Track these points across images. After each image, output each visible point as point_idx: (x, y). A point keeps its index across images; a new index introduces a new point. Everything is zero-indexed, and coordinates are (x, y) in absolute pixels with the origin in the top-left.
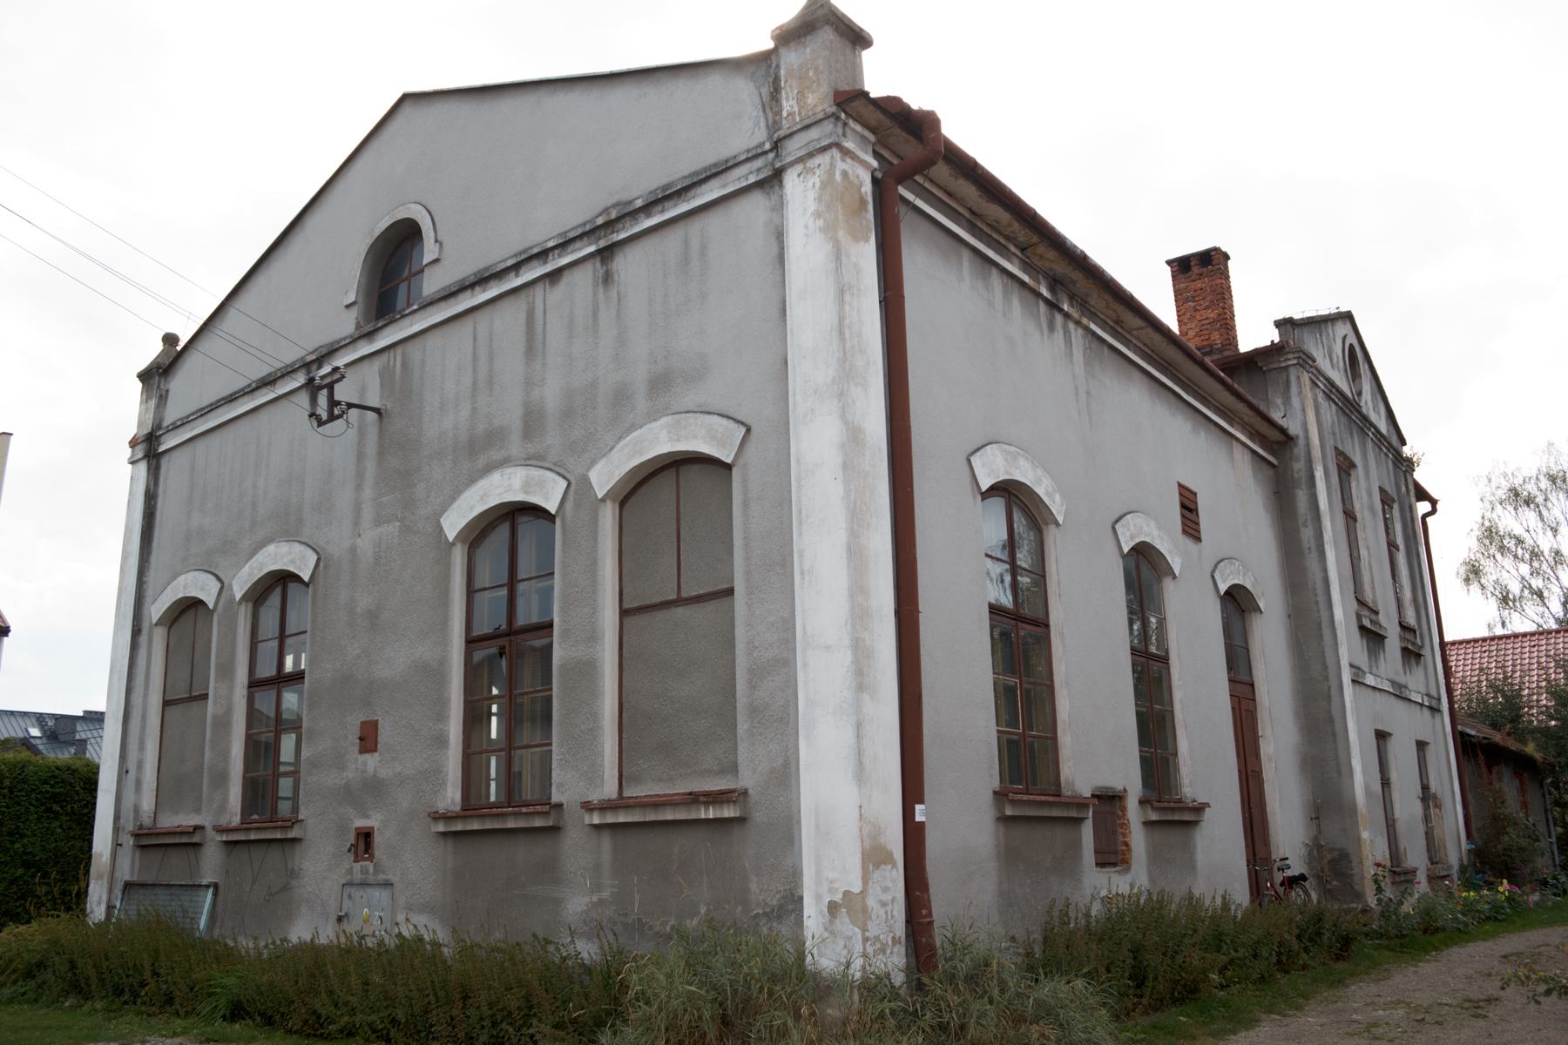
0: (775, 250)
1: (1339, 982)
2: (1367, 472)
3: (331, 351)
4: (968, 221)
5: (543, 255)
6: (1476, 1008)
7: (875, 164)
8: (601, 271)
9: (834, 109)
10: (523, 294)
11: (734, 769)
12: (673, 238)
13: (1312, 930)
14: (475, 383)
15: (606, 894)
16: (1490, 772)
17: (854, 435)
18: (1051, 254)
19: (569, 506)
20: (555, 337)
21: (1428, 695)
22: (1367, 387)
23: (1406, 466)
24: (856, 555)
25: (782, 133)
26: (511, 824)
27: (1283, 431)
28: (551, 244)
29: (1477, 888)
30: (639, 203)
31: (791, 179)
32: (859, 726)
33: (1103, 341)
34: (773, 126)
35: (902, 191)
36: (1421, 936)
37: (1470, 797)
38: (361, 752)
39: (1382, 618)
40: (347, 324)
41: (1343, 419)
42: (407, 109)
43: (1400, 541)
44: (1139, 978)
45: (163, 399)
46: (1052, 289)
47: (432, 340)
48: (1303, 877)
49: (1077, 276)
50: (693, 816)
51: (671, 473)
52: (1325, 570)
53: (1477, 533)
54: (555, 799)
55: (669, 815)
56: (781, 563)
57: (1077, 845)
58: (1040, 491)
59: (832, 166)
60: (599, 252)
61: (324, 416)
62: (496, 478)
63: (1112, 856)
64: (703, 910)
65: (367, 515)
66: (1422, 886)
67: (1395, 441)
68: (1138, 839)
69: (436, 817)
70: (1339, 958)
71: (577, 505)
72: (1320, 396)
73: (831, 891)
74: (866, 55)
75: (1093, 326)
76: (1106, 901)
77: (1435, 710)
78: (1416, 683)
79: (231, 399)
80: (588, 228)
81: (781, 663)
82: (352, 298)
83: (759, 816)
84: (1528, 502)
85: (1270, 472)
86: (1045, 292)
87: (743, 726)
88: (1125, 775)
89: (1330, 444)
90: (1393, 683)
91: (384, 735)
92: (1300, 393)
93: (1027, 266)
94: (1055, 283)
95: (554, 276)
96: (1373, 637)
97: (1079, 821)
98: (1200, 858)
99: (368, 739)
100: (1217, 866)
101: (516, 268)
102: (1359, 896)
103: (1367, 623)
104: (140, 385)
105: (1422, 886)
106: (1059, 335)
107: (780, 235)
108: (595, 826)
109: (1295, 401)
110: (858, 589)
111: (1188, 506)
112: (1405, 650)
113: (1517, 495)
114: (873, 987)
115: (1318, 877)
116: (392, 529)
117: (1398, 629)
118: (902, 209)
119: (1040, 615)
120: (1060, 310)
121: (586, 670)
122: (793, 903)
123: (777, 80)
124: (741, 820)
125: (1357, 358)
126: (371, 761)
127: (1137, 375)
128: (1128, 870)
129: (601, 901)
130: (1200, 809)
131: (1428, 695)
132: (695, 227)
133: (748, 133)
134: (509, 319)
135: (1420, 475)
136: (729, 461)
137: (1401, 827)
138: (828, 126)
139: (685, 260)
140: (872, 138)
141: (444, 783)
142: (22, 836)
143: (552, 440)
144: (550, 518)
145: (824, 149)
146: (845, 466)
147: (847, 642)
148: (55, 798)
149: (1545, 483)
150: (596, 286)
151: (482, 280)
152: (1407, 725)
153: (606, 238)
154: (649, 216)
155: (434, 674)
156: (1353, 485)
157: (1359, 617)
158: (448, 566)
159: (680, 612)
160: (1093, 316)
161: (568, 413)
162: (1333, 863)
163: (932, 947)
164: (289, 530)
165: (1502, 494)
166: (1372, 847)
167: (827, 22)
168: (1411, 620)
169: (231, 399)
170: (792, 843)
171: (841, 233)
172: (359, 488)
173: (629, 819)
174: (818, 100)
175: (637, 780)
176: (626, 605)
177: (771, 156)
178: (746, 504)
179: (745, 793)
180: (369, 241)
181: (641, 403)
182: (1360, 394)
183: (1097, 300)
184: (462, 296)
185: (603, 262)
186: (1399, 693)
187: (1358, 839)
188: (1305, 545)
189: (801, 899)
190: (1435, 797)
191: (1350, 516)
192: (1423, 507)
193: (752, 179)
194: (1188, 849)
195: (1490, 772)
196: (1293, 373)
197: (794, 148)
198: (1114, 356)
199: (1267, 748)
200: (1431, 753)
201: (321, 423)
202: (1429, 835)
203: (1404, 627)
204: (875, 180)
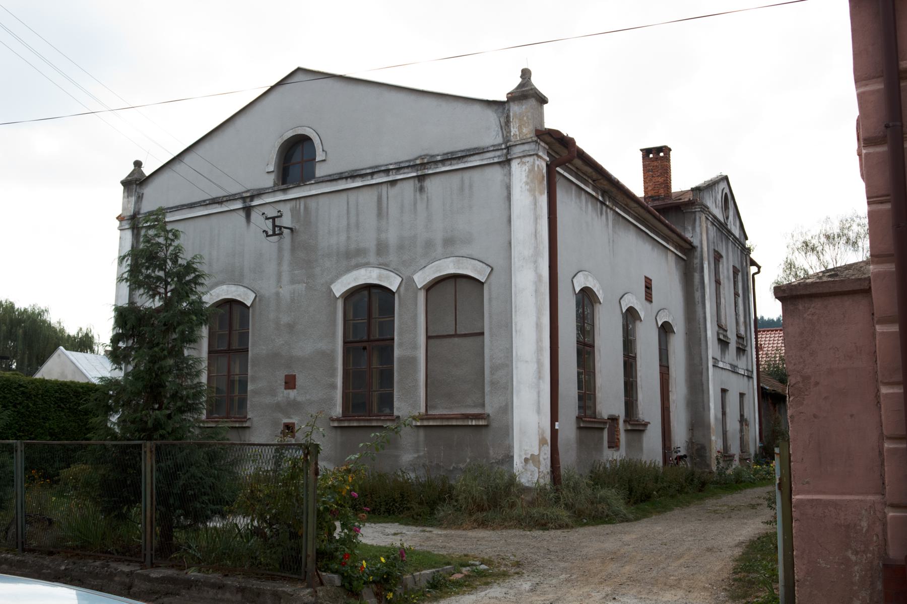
0: (505, 194)
1: (701, 499)
2: (728, 259)
3: (259, 193)
4: (576, 173)
5: (387, 171)
6: (753, 507)
7: (548, 159)
8: (418, 185)
9: (535, 139)
10: (375, 188)
11: (483, 405)
12: (455, 179)
13: (690, 478)
14: (348, 225)
15: (421, 454)
16: (775, 407)
17: (539, 277)
18: (605, 183)
19: (402, 289)
20: (393, 210)
21: (747, 370)
22: (731, 213)
23: (746, 251)
24: (538, 326)
25: (511, 143)
26: (374, 424)
27: (690, 243)
28: (391, 167)
29: (761, 465)
30: (439, 158)
31: (515, 164)
32: (539, 393)
33: (620, 215)
34: (506, 140)
35: (558, 169)
36: (737, 483)
37: (763, 419)
38: (286, 388)
39: (729, 334)
40: (269, 181)
41: (719, 234)
42: (300, 77)
43: (740, 292)
44: (631, 490)
45: (140, 198)
46: (603, 196)
47: (322, 200)
48: (685, 456)
49: (614, 190)
50: (466, 423)
51: (452, 282)
52: (705, 313)
53: (783, 266)
54: (396, 413)
55: (454, 423)
56: (507, 326)
57: (602, 438)
58: (595, 290)
59: (534, 163)
60: (418, 176)
61: (270, 233)
62: (362, 271)
63: (614, 444)
64: (468, 460)
65: (286, 278)
66: (736, 463)
67: (742, 240)
68: (622, 437)
69: (333, 420)
70: (700, 491)
71: (406, 289)
72: (709, 223)
73: (525, 454)
74: (545, 106)
75: (617, 210)
76: (611, 462)
77: (750, 377)
78: (742, 364)
79: (191, 206)
80: (412, 164)
81: (507, 364)
82: (272, 169)
83: (494, 425)
84: (813, 249)
85: (683, 263)
86: (600, 198)
87: (487, 389)
88: (619, 410)
89: (712, 248)
90: (731, 365)
91: (299, 381)
92: (700, 225)
93: (595, 188)
94: (604, 193)
95: (393, 183)
96: (723, 343)
97: (602, 429)
98: (645, 445)
99: (290, 382)
100: (651, 448)
101: (372, 174)
102: (709, 466)
103: (721, 337)
104: (122, 187)
105: (736, 463)
106: (604, 217)
107: (508, 188)
108: (417, 426)
109: (698, 229)
110: (539, 340)
111: (648, 287)
112: (738, 349)
113: (807, 245)
114: (542, 490)
115: (691, 457)
116: (301, 287)
117: (735, 337)
118: (558, 177)
119: (591, 342)
120: (605, 204)
121: (413, 361)
122: (509, 459)
123: (508, 117)
124: (486, 426)
125: (728, 200)
126: (292, 394)
127: (632, 227)
128: (618, 450)
129: (419, 457)
130: (646, 425)
131: (747, 370)
132: (467, 175)
133: (493, 137)
134: (368, 199)
135: (753, 256)
136: (483, 281)
137: (729, 435)
138: (533, 146)
139: (462, 189)
140: (547, 147)
141: (335, 405)
142: (49, 420)
143: (393, 258)
144: (393, 293)
145: (530, 155)
146: (536, 291)
147: (535, 360)
148: (61, 399)
149: (823, 239)
150: (415, 191)
151: (353, 175)
152: (736, 385)
153: (422, 169)
154: (444, 165)
155: (329, 356)
156: (721, 266)
157: (718, 334)
158: (335, 308)
159: (456, 339)
160: (616, 203)
161: (401, 247)
162: (698, 450)
163: (559, 475)
164: (236, 279)
165: (799, 244)
166: (716, 443)
167: (533, 96)
168: (742, 332)
169: (191, 206)
170: (508, 435)
171: (537, 193)
172: (280, 264)
173: (435, 424)
174: (528, 132)
175: (435, 407)
176: (429, 334)
177: (505, 151)
178: (490, 300)
179: (488, 415)
180: (280, 141)
181: (440, 249)
182: (727, 218)
183: (620, 197)
184: (340, 182)
185: (419, 181)
186: (734, 370)
187: (710, 440)
188: (697, 300)
189: (513, 457)
190: (746, 420)
191: (718, 282)
192: (753, 269)
193: (496, 160)
194: (640, 441)
195: (775, 407)
196: (698, 215)
197: (517, 151)
198: (624, 221)
199: (673, 397)
200: (746, 399)
201: (268, 236)
202: (742, 439)
203: (739, 337)
204: (547, 165)
